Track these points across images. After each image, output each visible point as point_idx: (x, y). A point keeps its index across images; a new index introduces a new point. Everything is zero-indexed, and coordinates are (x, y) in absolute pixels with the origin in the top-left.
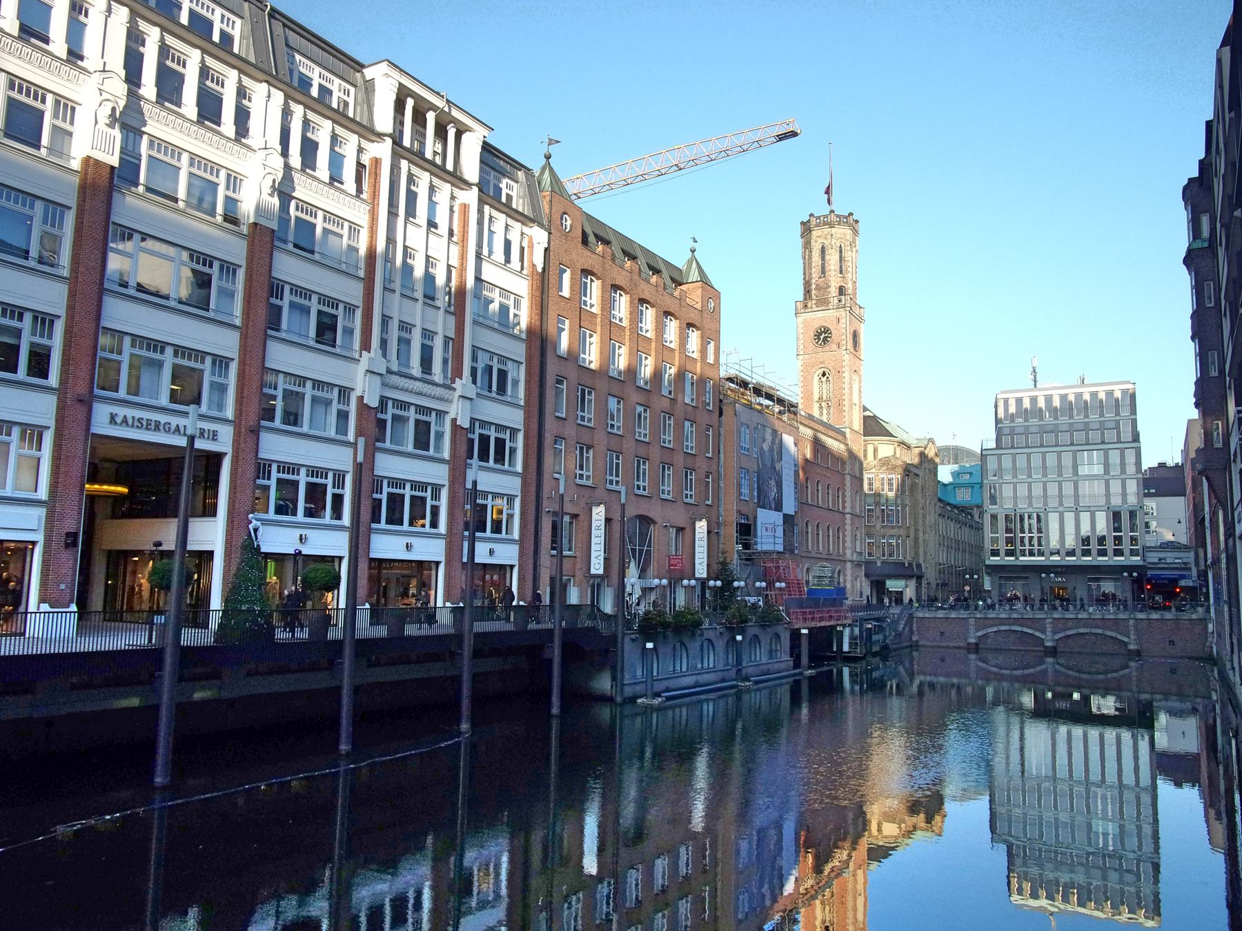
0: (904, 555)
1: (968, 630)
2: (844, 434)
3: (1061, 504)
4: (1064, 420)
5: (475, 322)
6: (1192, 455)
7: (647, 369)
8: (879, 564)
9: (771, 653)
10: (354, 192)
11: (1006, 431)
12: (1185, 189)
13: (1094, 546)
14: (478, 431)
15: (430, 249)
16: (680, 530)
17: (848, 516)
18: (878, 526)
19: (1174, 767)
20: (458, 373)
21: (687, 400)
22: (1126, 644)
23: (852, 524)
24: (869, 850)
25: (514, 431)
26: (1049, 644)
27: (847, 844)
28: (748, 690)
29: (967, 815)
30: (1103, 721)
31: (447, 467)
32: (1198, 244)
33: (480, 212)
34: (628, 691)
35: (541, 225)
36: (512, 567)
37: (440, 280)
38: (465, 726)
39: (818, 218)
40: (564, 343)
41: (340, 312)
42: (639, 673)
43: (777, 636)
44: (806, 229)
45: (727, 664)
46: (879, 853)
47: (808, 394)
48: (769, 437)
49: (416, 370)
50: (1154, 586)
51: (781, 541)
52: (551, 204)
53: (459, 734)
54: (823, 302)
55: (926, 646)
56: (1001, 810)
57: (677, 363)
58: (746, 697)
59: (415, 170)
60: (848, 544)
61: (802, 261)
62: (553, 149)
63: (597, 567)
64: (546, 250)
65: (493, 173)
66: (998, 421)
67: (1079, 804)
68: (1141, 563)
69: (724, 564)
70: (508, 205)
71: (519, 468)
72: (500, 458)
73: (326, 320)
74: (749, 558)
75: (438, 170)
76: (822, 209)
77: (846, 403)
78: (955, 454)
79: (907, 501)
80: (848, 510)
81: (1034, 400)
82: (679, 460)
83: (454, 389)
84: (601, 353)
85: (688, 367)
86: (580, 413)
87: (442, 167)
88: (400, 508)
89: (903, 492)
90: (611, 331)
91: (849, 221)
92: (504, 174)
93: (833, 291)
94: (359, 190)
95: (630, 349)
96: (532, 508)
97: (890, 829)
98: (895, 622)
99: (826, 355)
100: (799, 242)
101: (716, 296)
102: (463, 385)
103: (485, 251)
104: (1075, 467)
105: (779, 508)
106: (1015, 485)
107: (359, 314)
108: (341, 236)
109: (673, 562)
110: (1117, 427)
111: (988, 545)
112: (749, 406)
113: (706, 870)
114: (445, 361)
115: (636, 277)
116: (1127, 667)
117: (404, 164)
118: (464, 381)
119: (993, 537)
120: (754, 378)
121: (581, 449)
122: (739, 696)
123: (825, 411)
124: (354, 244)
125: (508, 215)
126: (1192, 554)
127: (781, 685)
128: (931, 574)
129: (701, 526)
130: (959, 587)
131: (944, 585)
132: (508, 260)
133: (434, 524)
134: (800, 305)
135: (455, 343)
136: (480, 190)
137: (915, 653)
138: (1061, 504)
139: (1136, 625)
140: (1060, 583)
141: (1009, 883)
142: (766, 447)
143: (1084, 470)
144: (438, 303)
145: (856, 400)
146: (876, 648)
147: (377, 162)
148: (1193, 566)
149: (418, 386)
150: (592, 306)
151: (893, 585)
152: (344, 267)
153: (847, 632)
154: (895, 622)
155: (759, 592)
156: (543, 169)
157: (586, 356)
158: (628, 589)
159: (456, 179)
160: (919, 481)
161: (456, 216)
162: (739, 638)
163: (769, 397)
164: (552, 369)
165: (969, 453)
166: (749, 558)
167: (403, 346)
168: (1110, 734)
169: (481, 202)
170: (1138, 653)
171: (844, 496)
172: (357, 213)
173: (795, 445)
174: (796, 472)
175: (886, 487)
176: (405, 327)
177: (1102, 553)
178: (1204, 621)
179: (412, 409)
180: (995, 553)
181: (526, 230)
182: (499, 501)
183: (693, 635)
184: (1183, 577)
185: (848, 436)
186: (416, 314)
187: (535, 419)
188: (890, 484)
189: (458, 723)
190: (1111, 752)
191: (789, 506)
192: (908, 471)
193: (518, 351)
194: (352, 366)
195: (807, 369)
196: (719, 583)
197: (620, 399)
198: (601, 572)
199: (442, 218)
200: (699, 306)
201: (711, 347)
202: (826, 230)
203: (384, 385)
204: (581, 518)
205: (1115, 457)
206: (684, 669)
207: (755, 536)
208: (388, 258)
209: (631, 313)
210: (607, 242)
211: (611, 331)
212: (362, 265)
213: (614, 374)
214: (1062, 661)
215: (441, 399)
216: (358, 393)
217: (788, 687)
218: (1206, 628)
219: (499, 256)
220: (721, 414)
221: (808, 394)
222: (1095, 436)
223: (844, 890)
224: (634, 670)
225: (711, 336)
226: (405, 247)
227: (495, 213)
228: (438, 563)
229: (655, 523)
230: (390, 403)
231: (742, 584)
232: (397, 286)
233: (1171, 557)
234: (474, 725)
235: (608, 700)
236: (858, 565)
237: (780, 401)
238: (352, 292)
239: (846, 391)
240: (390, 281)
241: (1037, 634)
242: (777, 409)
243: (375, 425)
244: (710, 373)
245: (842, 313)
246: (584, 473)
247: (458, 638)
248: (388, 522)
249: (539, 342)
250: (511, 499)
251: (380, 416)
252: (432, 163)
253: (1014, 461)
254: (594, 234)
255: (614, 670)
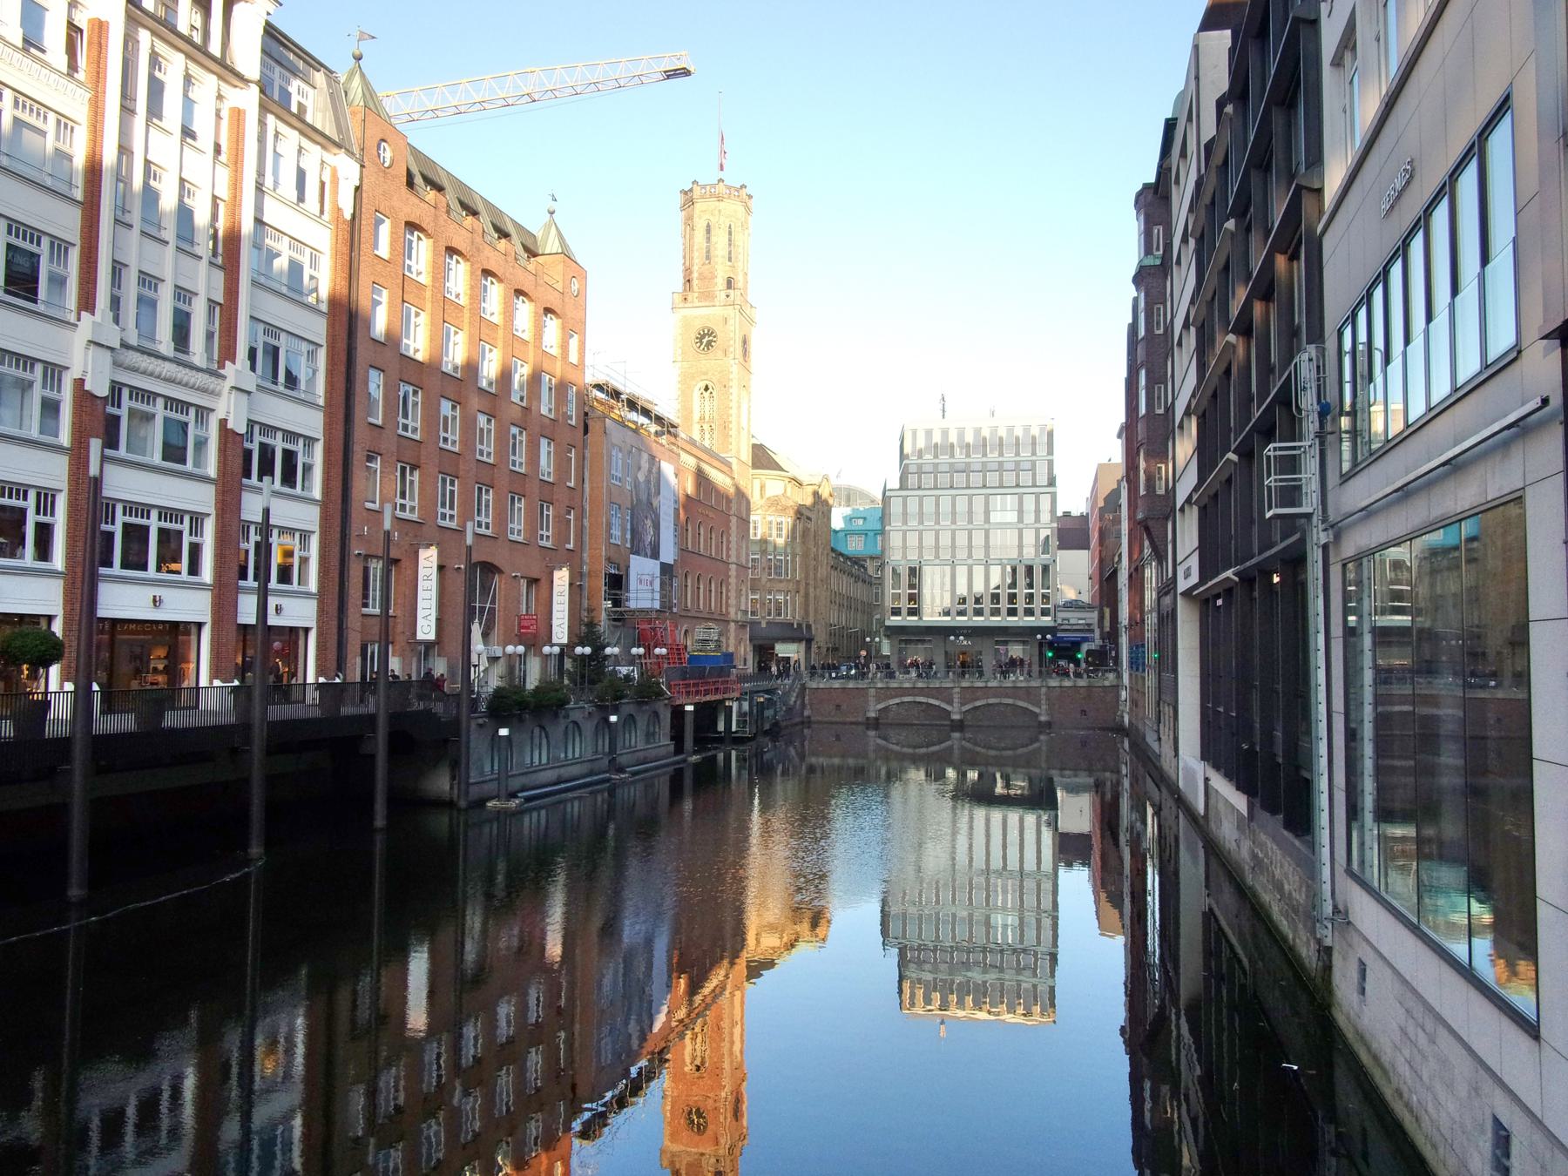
0: (792, 615)
1: (867, 702)
2: (729, 465)
3: (970, 556)
4: (976, 457)
5: (255, 283)
6: (1101, 504)
7: (490, 369)
8: (764, 625)
9: (649, 736)
10: (65, 70)
11: (913, 469)
12: (1139, 195)
13: (987, 605)
14: (258, 438)
15: (184, 166)
16: (532, 581)
17: (733, 567)
18: (764, 580)
19: (1071, 849)
20: (228, 353)
21: (544, 411)
22: (1037, 715)
23: (737, 577)
24: (748, 967)
25: (310, 441)
26: (956, 717)
27: (726, 962)
28: (623, 783)
29: (854, 917)
30: (1007, 801)
31: (213, 488)
32: (1150, 261)
33: (262, 123)
34: (475, 792)
35: (350, 153)
36: (307, 630)
37: (202, 218)
38: (256, 850)
39: (704, 187)
40: (380, 325)
41: (44, 249)
42: (487, 768)
43: (656, 714)
44: (688, 199)
45: (596, 752)
46: (756, 970)
47: (687, 410)
48: (645, 465)
49: (165, 345)
50: (1058, 648)
51: (657, 596)
52: (363, 130)
53: (248, 862)
54: (707, 296)
55: (819, 722)
56: (894, 909)
57: (531, 358)
58: (619, 791)
59: (161, 48)
60: (732, 601)
61: (681, 240)
62: (366, 48)
63: (426, 630)
64: (357, 189)
65: (278, 69)
66: (903, 456)
67: (979, 897)
68: (1052, 624)
69: (591, 625)
70: (300, 117)
71: (317, 493)
72: (289, 478)
73: (22, 261)
74: (620, 618)
75: (197, 51)
76: (709, 176)
77: (733, 426)
78: (849, 496)
79: (798, 550)
80: (733, 559)
81: (945, 433)
82: (533, 489)
83: (224, 377)
84: (432, 340)
85: (546, 366)
86: (402, 420)
87: (203, 49)
88: (152, 545)
89: (794, 538)
90: (445, 311)
91: (741, 193)
92: (295, 73)
93: (721, 283)
94: (73, 66)
95: (471, 337)
96: (336, 550)
97: (771, 941)
98: (787, 694)
99: (710, 363)
100: (680, 217)
101: (580, 273)
102: (236, 371)
103: (269, 182)
104: (987, 513)
105: (655, 554)
106: (905, 532)
107: (74, 256)
108: (43, 134)
109: (525, 623)
110: (1033, 469)
111: (889, 603)
112: (622, 423)
113: (560, 1015)
114: (210, 336)
115: (479, 239)
116: (1037, 740)
117: (144, 36)
118: (238, 365)
119: (895, 593)
120: (628, 388)
121: (403, 470)
122: (612, 792)
123: (707, 436)
124: (65, 148)
125: (302, 133)
126: (1095, 615)
127: (658, 776)
128: (821, 637)
129: (562, 578)
130: (847, 651)
131: (835, 649)
132: (301, 199)
133: (194, 569)
134: (678, 298)
135: (226, 311)
136: (262, 91)
137: (806, 731)
138: (970, 556)
139: (1041, 693)
140: (961, 646)
141: (900, 991)
142: (641, 477)
143: (995, 517)
144: (198, 250)
145: (744, 423)
146: (767, 727)
147: (100, 27)
148: (1096, 627)
149: (168, 369)
150: (419, 274)
151: (784, 650)
152: (49, 182)
153: (735, 706)
154: (787, 694)
155: (632, 660)
156: (351, 75)
157: (410, 342)
158: (474, 660)
159: (225, 69)
160: (811, 526)
161: (225, 124)
162: (613, 719)
163: (646, 412)
164: (363, 353)
165: (863, 495)
166: (620, 618)
167: (145, 310)
168: (1014, 816)
169: (264, 108)
170: (1049, 724)
171: (729, 542)
172: (72, 101)
173: (676, 476)
174: (677, 511)
175: (774, 532)
176: (148, 280)
177: (979, 612)
178: (1116, 688)
179: (160, 402)
180: (896, 612)
181: (328, 157)
182: (286, 539)
183: (556, 715)
184: (1086, 640)
185: (735, 467)
186: (165, 263)
187: (340, 427)
188: (780, 529)
189: (245, 846)
190: (1013, 834)
191: (668, 554)
192: (801, 514)
193: (317, 329)
194: (65, 332)
195: (686, 380)
196: (588, 650)
197: (456, 403)
198: (432, 636)
199: (203, 124)
200: (559, 286)
201: (574, 343)
202: (713, 204)
203: (117, 364)
204: (404, 564)
205: (1029, 503)
206: (544, 760)
207: (628, 591)
208: (122, 178)
209: (472, 288)
210: (440, 189)
211: (445, 311)
212: (79, 181)
213: (448, 368)
214: (968, 735)
215: (204, 390)
216: (75, 373)
217: (667, 778)
218: (1118, 696)
219: (288, 189)
220: (586, 431)
221: (687, 410)
222: (1009, 479)
223: (719, 1018)
224: (482, 766)
225: (574, 327)
226: (147, 163)
227: (282, 128)
228: (200, 625)
229: (500, 572)
230: (125, 393)
231: (616, 650)
232: (135, 218)
233: (1075, 618)
234: (269, 844)
235: (450, 804)
236: (743, 626)
237: (659, 420)
238: (66, 222)
239: (733, 412)
240: (124, 211)
241: (944, 705)
242: (654, 428)
243: (101, 421)
244: (572, 376)
245: (730, 311)
246: (407, 502)
247: (243, 727)
248: (124, 566)
249: (346, 319)
250: (305, 536)
251: (110, 410)
252: (188, 40)
253: (921, 505)
254: (424, 177)
255: (455, 765)
